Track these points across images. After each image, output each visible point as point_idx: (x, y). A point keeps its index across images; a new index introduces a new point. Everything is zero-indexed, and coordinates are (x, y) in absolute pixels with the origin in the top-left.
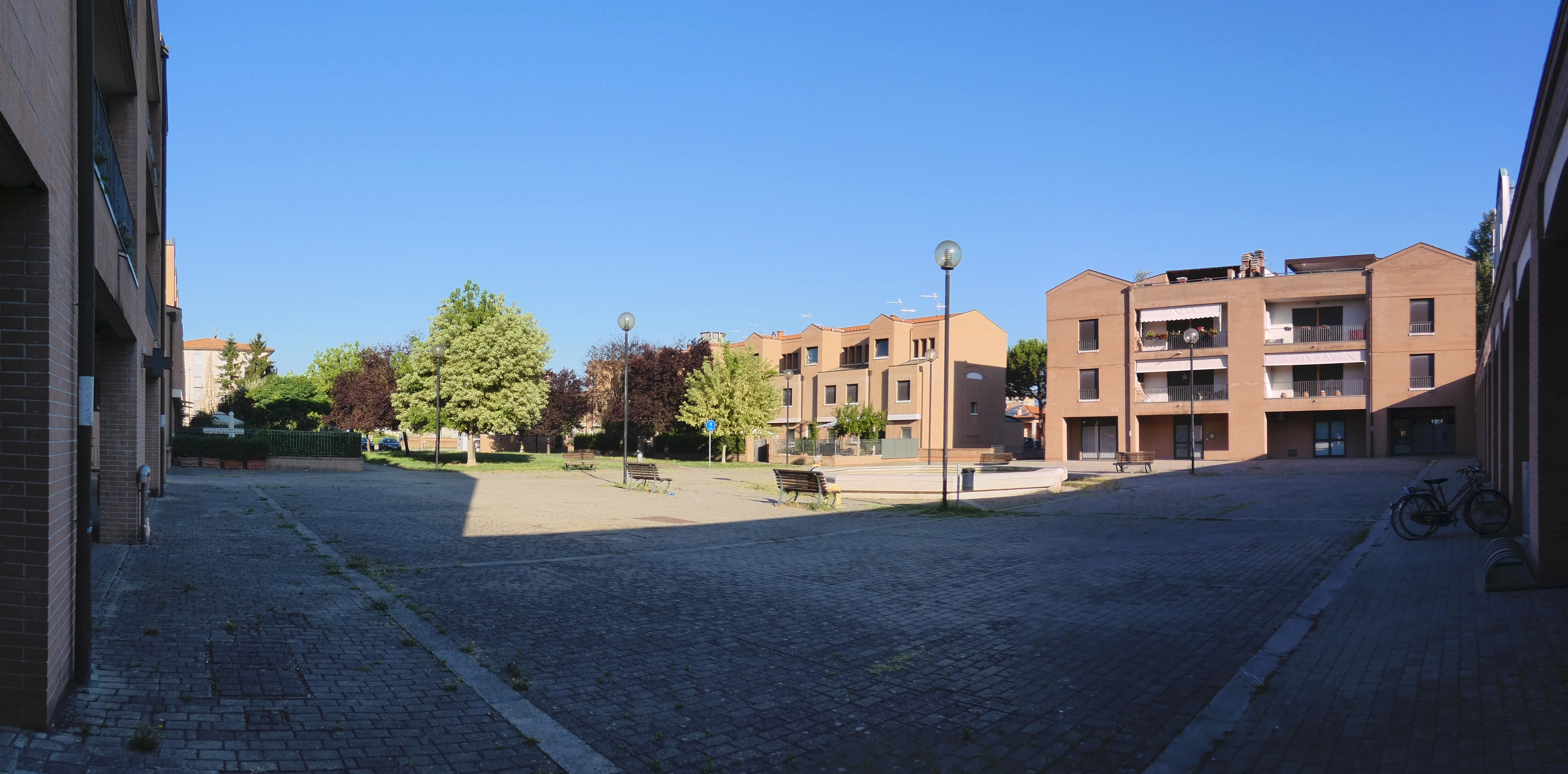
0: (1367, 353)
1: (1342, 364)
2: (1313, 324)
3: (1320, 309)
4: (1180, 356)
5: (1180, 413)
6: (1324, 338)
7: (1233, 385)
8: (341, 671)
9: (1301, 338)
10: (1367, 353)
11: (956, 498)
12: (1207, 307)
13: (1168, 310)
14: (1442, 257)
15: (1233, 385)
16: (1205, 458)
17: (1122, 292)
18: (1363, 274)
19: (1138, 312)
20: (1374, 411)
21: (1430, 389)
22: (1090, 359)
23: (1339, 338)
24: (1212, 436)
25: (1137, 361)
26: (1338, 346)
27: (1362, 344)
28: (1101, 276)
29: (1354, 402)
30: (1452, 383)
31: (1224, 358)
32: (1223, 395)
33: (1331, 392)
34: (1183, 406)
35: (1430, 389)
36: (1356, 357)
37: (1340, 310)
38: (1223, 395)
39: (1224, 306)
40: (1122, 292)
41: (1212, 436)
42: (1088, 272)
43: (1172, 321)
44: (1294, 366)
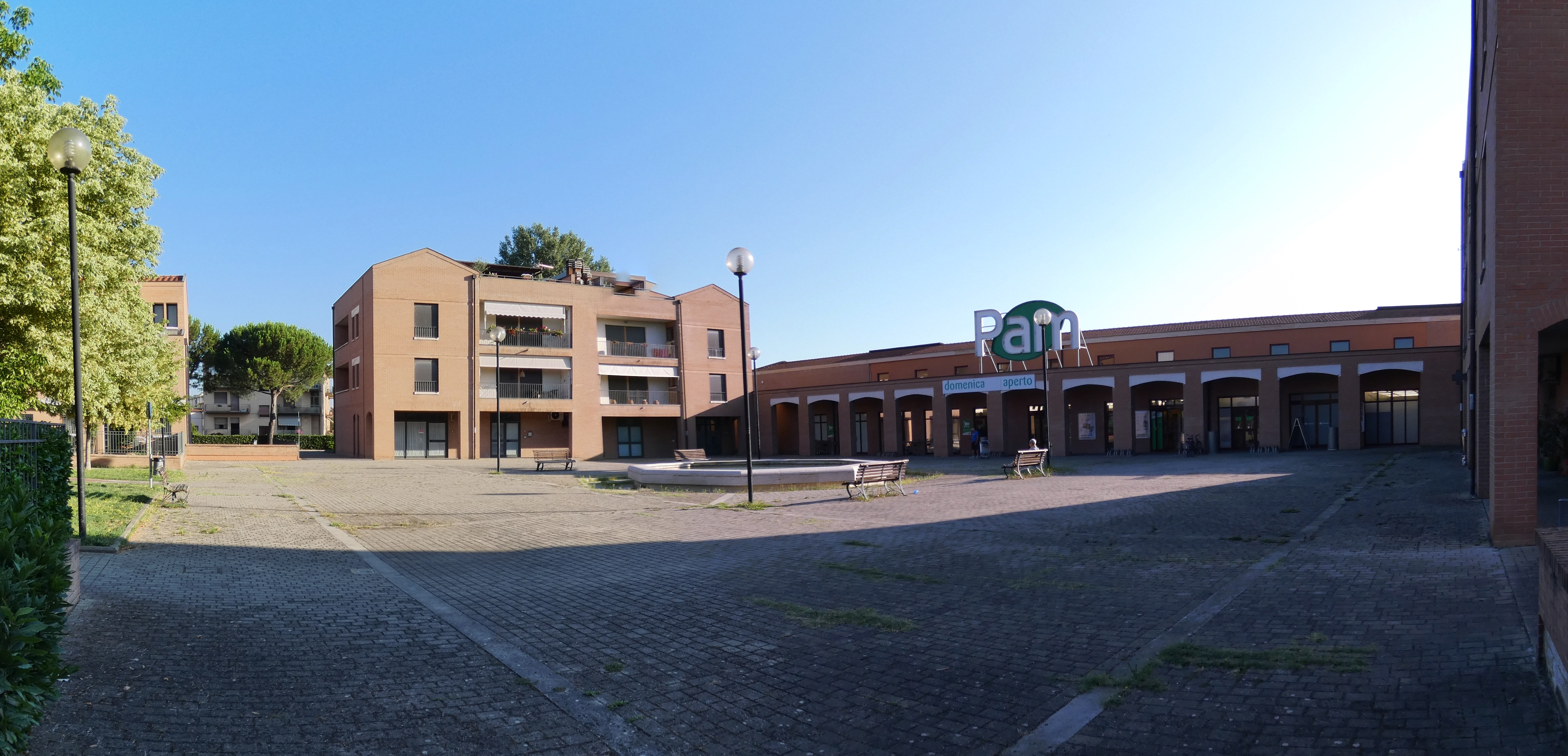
0: (679, 369)
1: (646, 378)
2: (622, 340)
3: (627, 327)
4: (527, 353)
5: (527, 411)
6: (630, 353)
7: (577, 385)
8: (690, 641)
9: (614, 351)
10: (679, 369)
11: (1233, 399)
12: (551, 308)
13: (513, 305)
14: (728, 298)
15: (577, 385)
16: (522, 455)
17: (466, 279)
18: (674, 303)
19: (482, 304)
20: (688, 417)
21: (724, 402)
22: (428, 347)
23: (644, 354)
24: (530, 434)
25: (482, 354)
26: (658, 363)
27: (674, 361)
28: (442, 257)
29: (671, 411)
30: (736, 399)
31: (569, 359)
32: (567, 394)
33: (638, 401)
34: (530, 403)
35: (724, 402)
36: (669, 373)
37: (643, 330)
38: (567, 394)
39: (568, 309)
40: (466, 279)
41: (530, 434)
42: (426, 250)
43: (524, 317)
44: (609, 376)
